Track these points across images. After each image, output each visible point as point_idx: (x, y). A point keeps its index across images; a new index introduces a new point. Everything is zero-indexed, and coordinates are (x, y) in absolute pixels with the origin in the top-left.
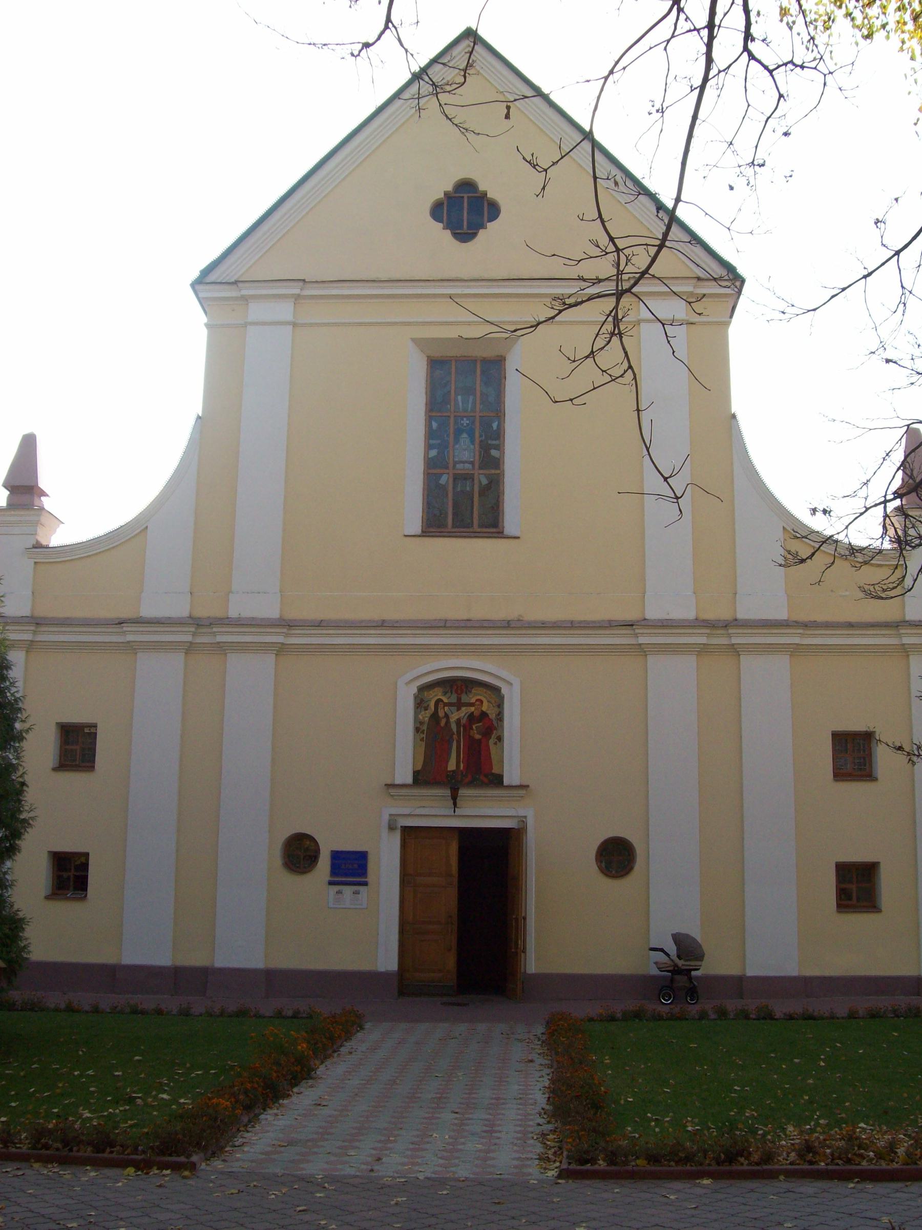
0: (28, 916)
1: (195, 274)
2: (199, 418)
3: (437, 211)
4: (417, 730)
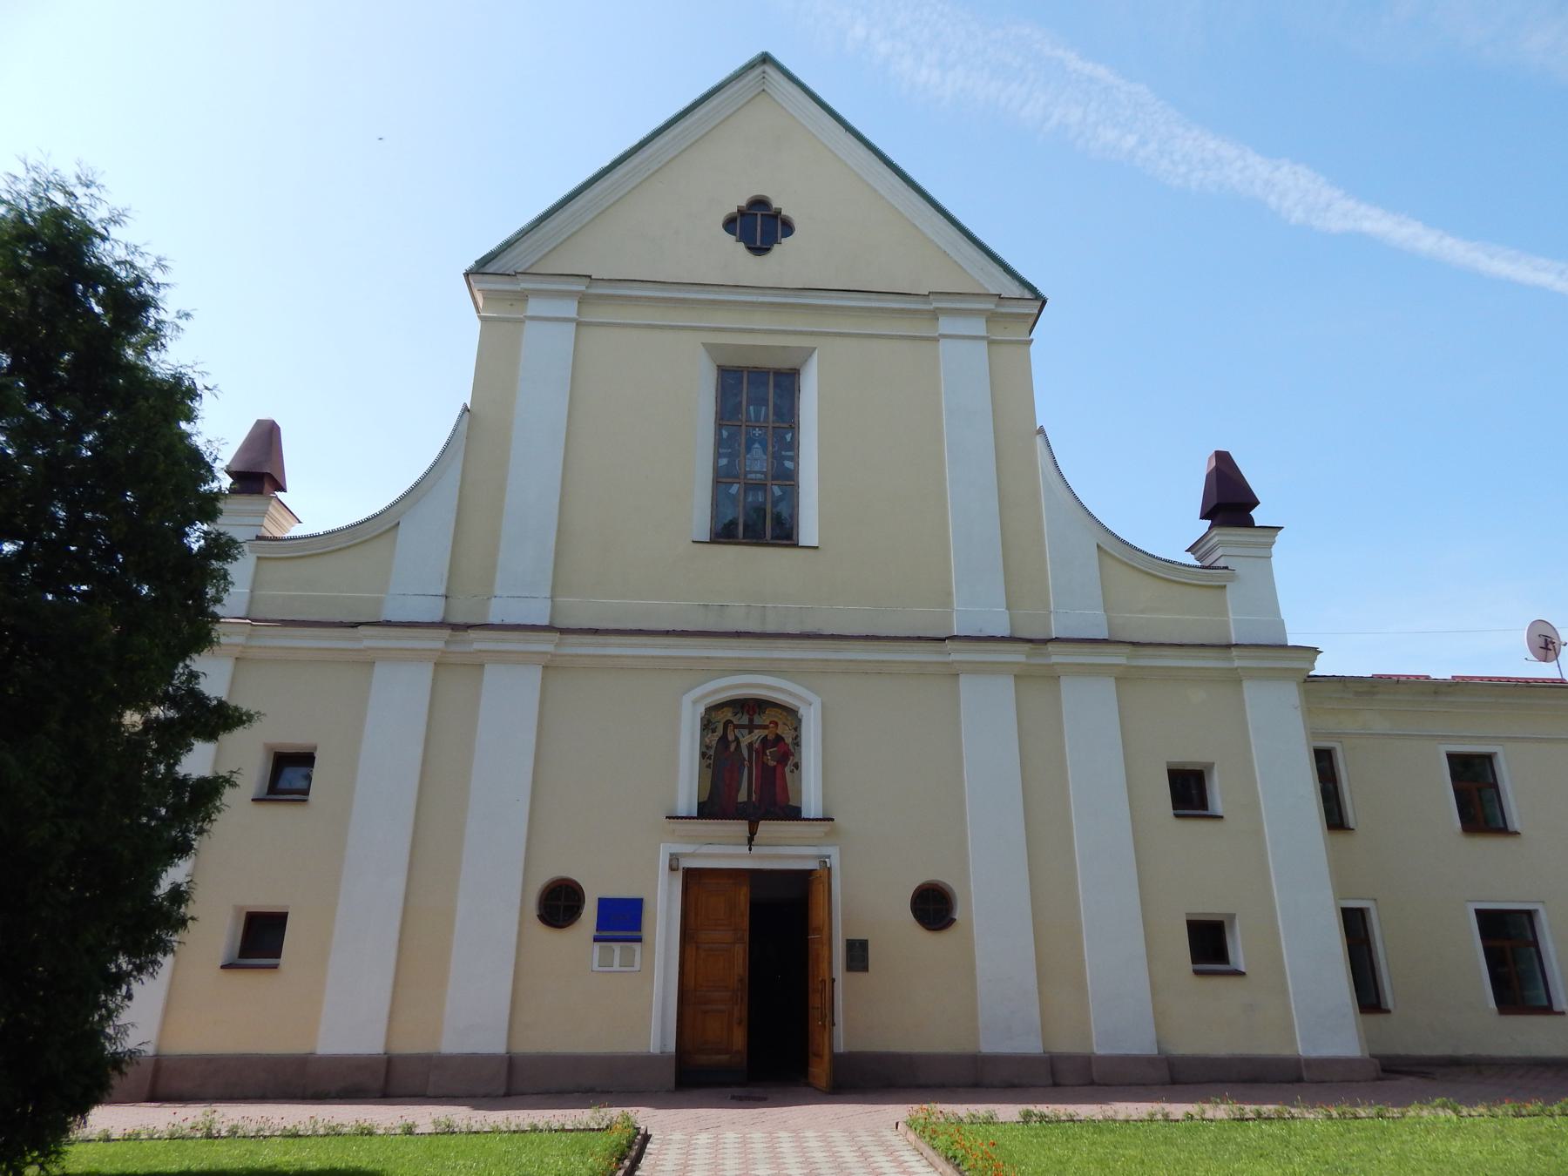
0: (201, 414)
1: (470, 263)
2: (466, 409)
3: (729, 224)
4: (703, 755)
